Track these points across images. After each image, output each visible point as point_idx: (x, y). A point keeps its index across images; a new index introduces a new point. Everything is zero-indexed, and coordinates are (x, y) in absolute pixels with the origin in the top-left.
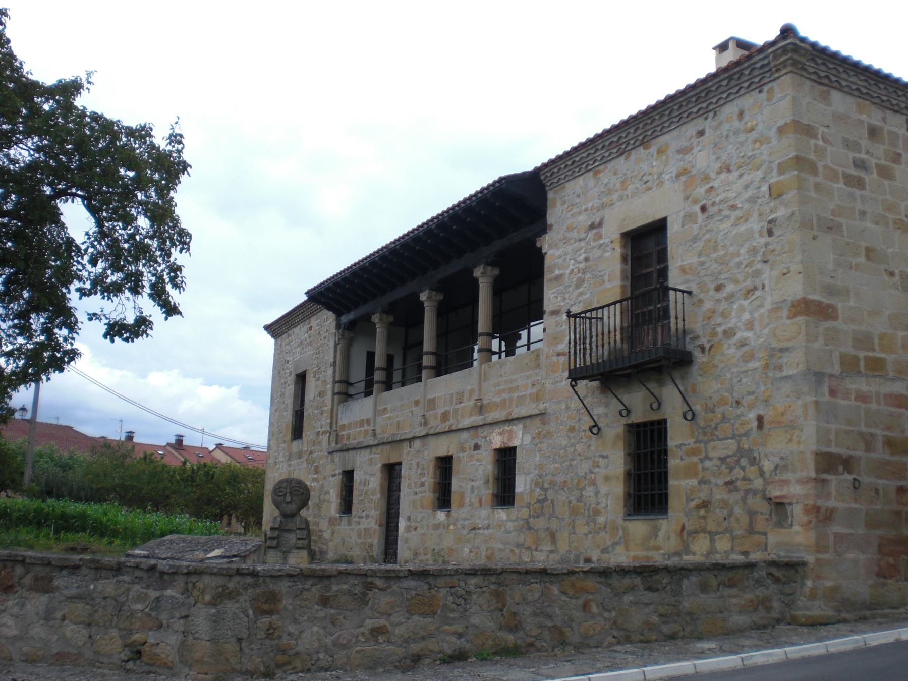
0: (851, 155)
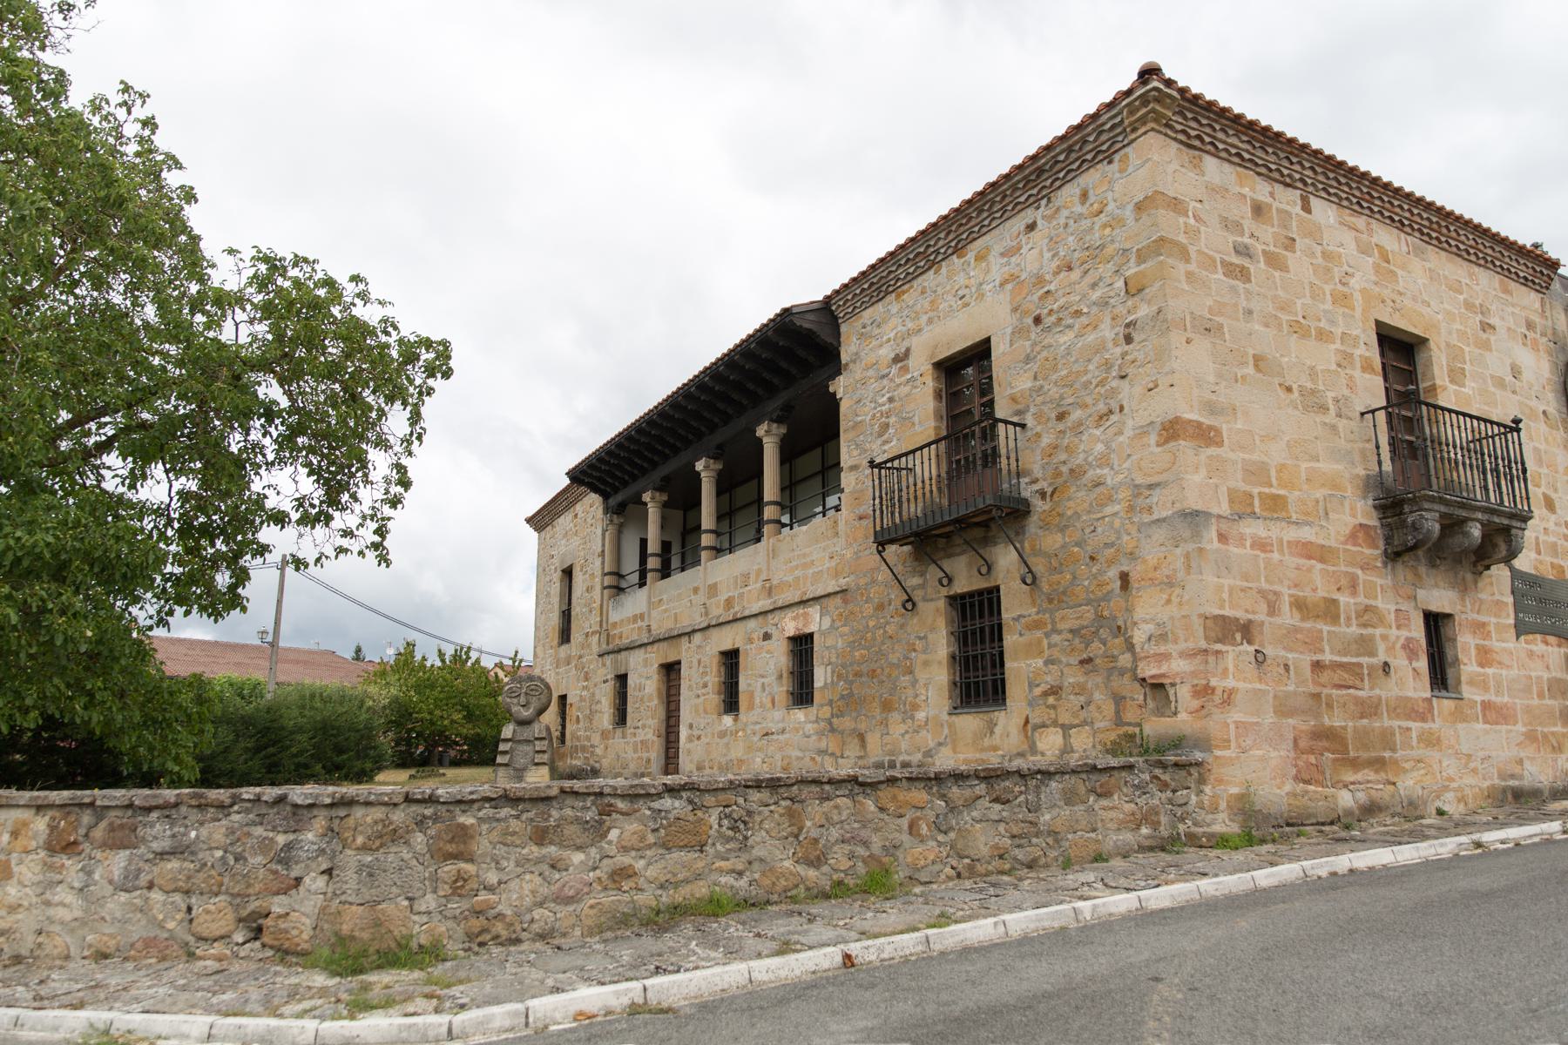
0: (1231, 238)
